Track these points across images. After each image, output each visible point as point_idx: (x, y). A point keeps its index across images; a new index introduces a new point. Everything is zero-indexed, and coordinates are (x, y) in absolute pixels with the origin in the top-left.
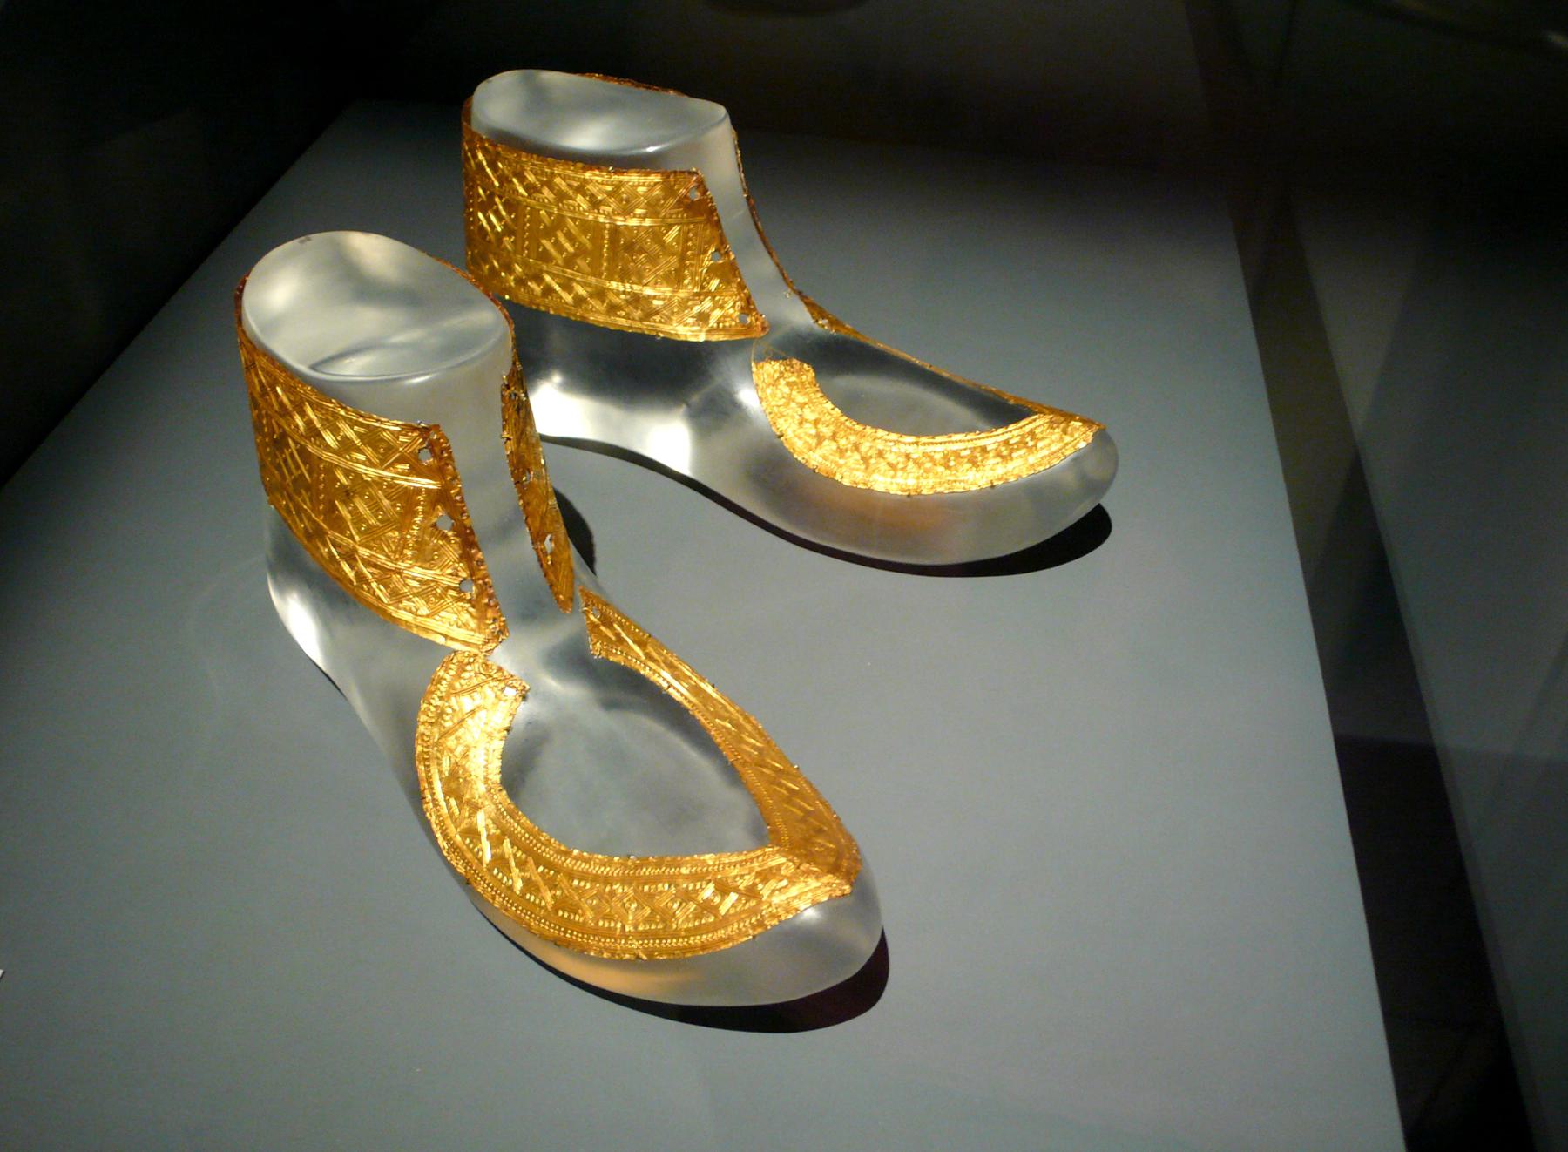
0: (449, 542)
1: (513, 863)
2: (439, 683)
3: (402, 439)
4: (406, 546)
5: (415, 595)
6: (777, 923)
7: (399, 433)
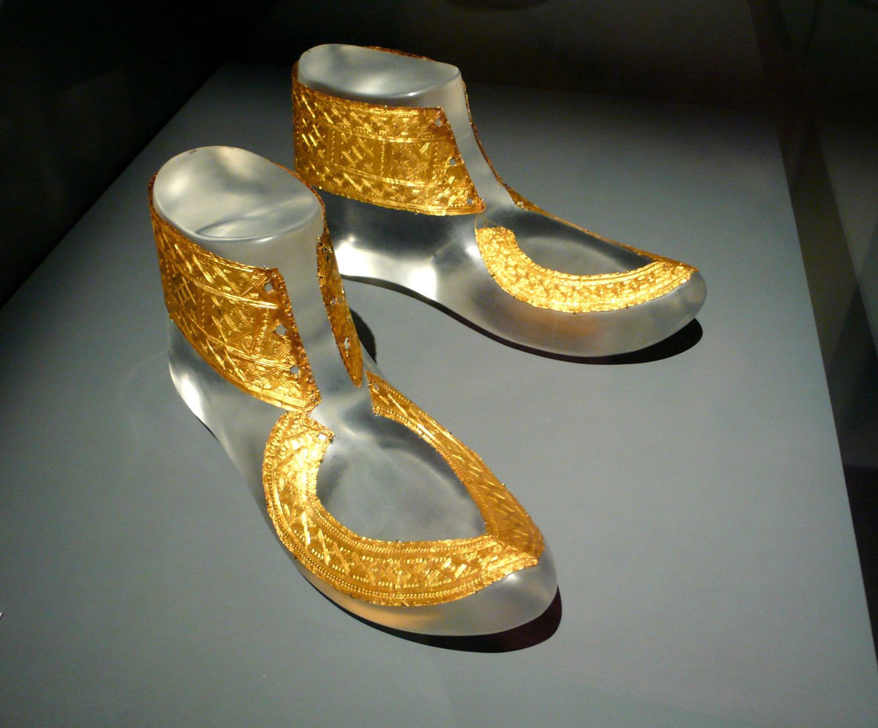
2: (278, 431)
3: (254, 277)
5: (262, 376)
7: (252, 274)
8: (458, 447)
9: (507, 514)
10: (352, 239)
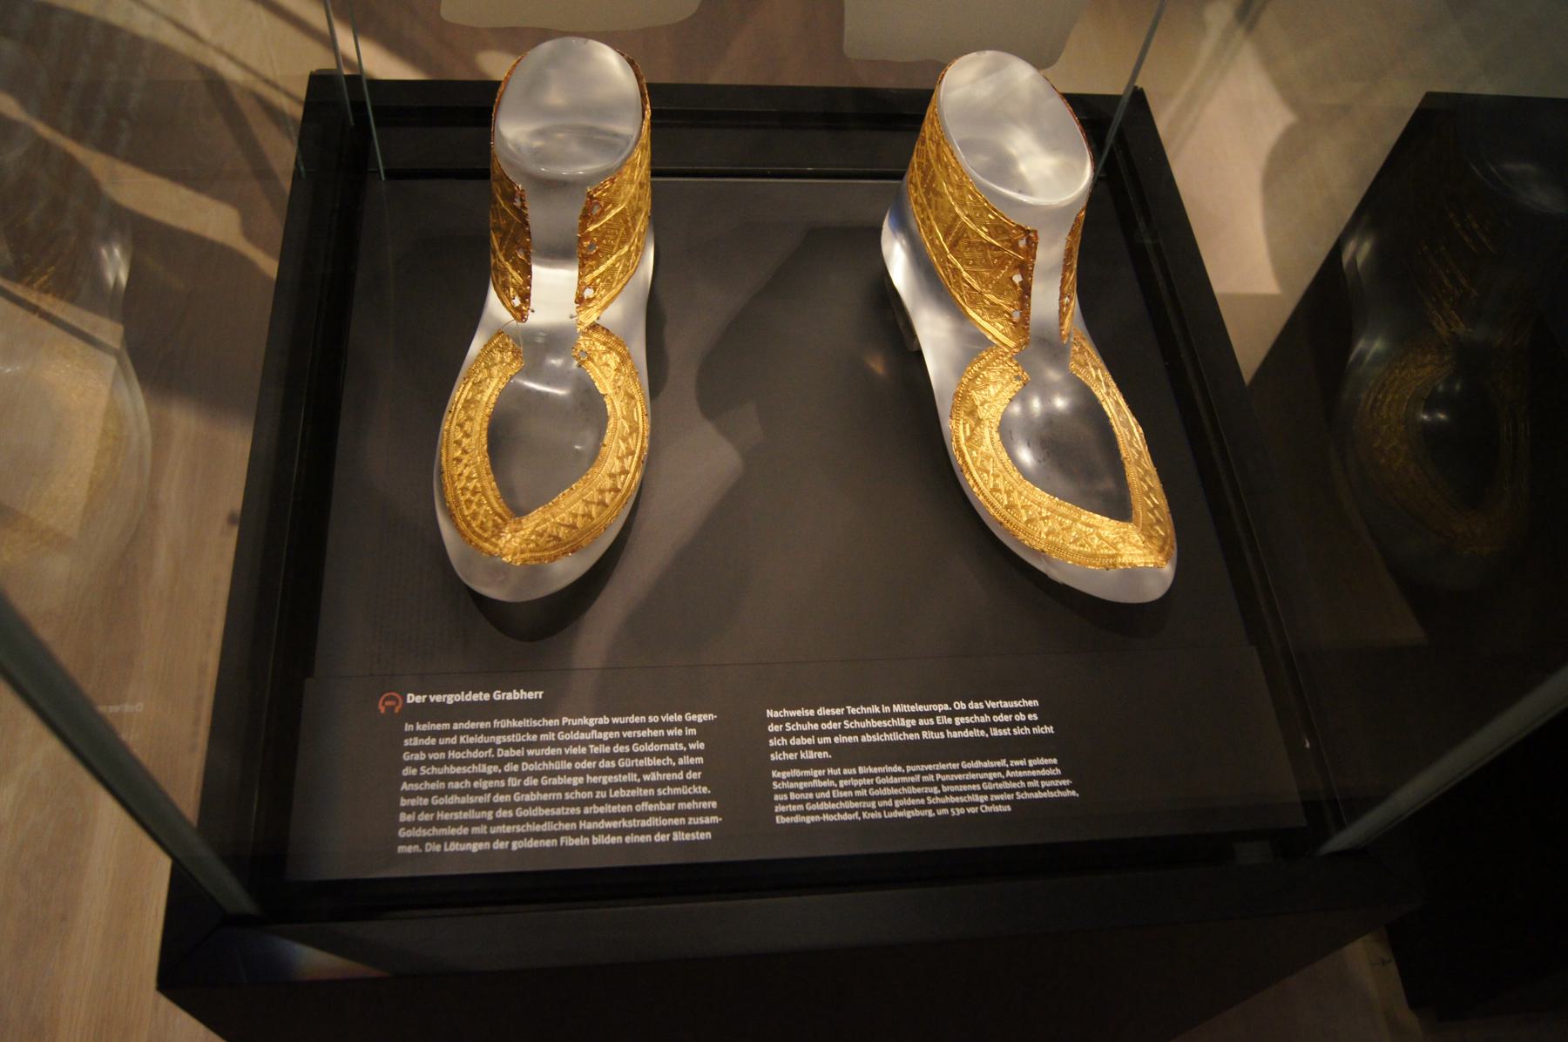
0: (1016, 289)
1: (521, 342)
2: (981, 359)
3: (1014, 231)
4: (991, 283)
5: (985, 308)
6: (907, 767)
7: (1014, 228)
8: (1137, 442)
9: (1152, 506)
10: (1036, 416)
